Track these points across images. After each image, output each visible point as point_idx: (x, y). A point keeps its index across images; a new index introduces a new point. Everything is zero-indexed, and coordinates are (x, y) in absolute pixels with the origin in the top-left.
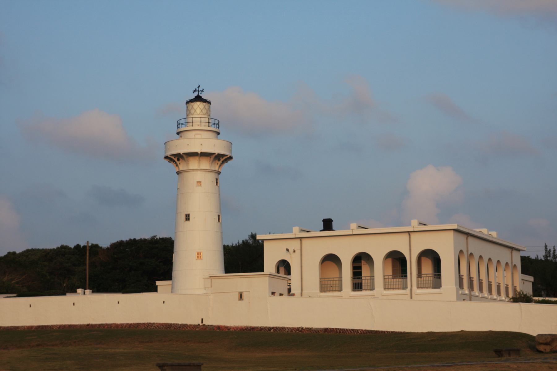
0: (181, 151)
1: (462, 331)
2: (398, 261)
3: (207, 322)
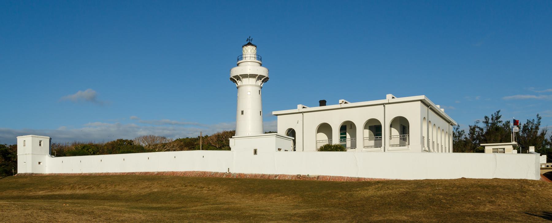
1: (463, 178)
2: (375, 128)
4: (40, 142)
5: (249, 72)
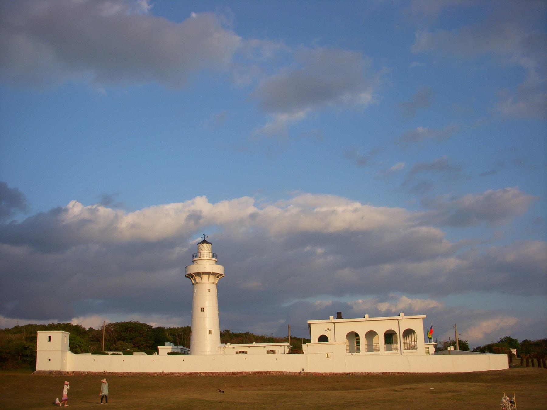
0: (201, 271)
3: (305, 371)
4: (50, 337)
5: (208, 270)
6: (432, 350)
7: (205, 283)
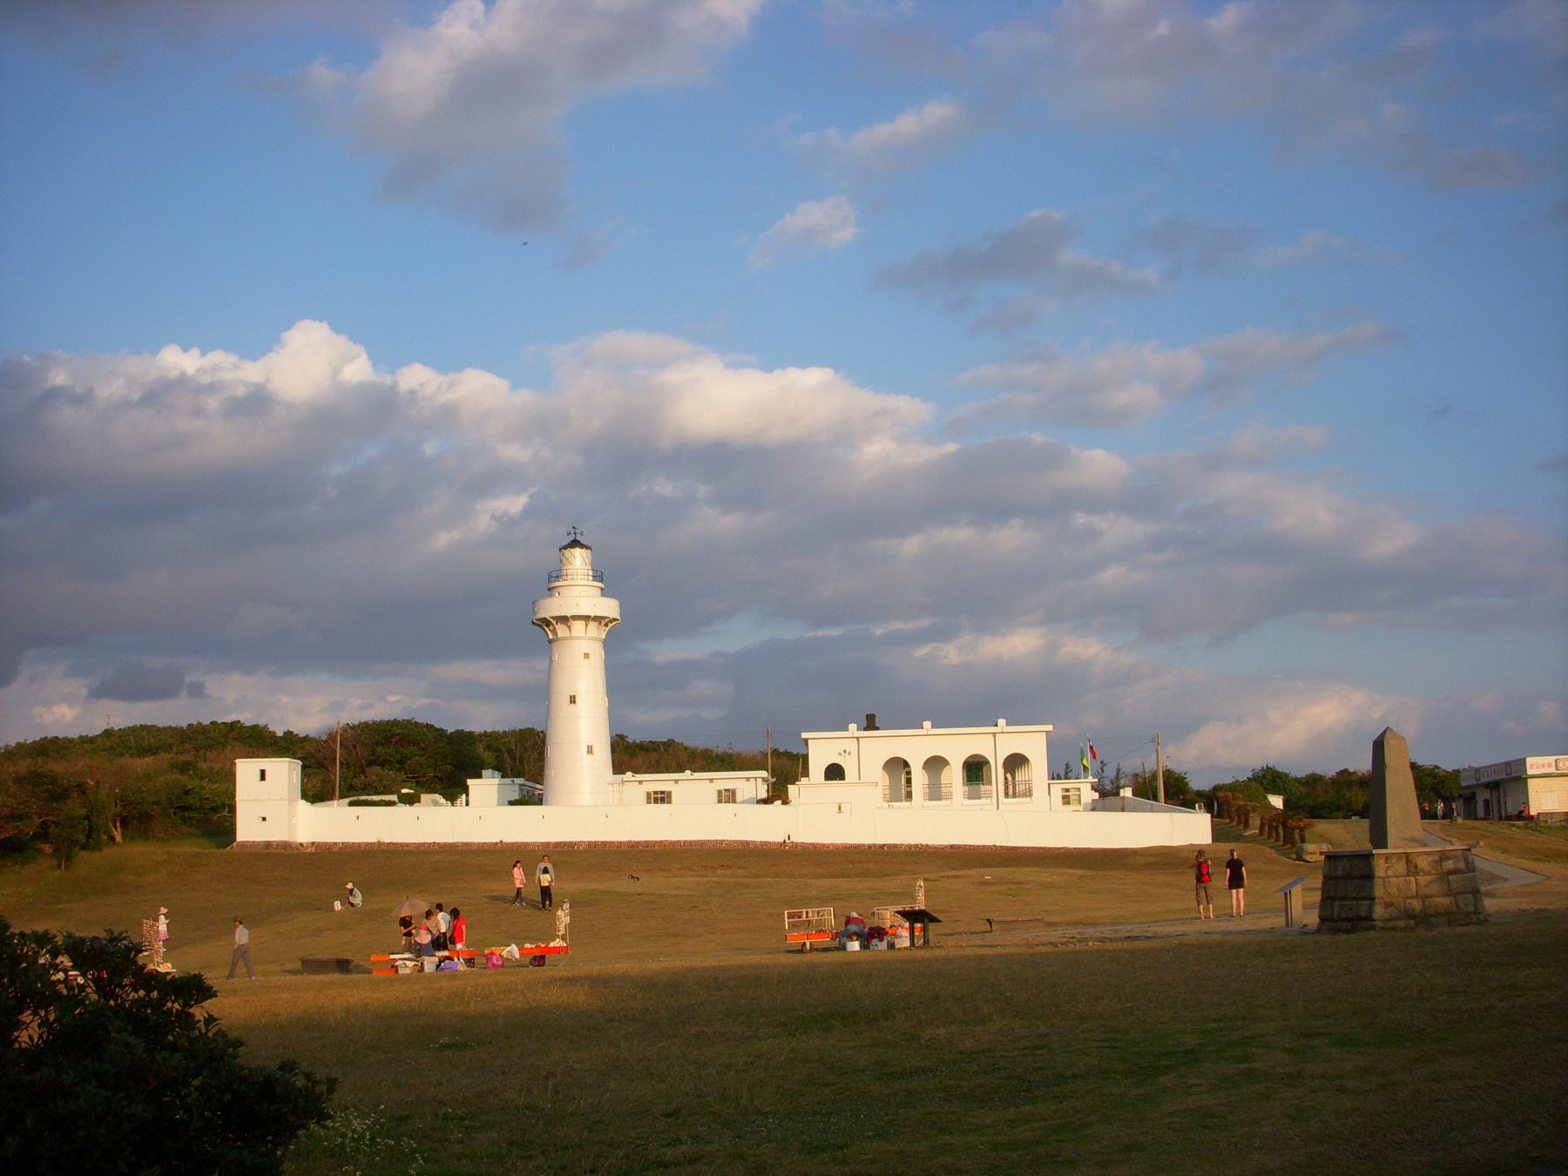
4: (263, 773)
6: (1089, 795)
7: (578, 638)
